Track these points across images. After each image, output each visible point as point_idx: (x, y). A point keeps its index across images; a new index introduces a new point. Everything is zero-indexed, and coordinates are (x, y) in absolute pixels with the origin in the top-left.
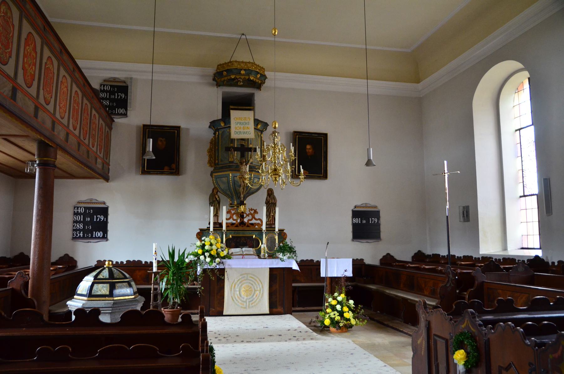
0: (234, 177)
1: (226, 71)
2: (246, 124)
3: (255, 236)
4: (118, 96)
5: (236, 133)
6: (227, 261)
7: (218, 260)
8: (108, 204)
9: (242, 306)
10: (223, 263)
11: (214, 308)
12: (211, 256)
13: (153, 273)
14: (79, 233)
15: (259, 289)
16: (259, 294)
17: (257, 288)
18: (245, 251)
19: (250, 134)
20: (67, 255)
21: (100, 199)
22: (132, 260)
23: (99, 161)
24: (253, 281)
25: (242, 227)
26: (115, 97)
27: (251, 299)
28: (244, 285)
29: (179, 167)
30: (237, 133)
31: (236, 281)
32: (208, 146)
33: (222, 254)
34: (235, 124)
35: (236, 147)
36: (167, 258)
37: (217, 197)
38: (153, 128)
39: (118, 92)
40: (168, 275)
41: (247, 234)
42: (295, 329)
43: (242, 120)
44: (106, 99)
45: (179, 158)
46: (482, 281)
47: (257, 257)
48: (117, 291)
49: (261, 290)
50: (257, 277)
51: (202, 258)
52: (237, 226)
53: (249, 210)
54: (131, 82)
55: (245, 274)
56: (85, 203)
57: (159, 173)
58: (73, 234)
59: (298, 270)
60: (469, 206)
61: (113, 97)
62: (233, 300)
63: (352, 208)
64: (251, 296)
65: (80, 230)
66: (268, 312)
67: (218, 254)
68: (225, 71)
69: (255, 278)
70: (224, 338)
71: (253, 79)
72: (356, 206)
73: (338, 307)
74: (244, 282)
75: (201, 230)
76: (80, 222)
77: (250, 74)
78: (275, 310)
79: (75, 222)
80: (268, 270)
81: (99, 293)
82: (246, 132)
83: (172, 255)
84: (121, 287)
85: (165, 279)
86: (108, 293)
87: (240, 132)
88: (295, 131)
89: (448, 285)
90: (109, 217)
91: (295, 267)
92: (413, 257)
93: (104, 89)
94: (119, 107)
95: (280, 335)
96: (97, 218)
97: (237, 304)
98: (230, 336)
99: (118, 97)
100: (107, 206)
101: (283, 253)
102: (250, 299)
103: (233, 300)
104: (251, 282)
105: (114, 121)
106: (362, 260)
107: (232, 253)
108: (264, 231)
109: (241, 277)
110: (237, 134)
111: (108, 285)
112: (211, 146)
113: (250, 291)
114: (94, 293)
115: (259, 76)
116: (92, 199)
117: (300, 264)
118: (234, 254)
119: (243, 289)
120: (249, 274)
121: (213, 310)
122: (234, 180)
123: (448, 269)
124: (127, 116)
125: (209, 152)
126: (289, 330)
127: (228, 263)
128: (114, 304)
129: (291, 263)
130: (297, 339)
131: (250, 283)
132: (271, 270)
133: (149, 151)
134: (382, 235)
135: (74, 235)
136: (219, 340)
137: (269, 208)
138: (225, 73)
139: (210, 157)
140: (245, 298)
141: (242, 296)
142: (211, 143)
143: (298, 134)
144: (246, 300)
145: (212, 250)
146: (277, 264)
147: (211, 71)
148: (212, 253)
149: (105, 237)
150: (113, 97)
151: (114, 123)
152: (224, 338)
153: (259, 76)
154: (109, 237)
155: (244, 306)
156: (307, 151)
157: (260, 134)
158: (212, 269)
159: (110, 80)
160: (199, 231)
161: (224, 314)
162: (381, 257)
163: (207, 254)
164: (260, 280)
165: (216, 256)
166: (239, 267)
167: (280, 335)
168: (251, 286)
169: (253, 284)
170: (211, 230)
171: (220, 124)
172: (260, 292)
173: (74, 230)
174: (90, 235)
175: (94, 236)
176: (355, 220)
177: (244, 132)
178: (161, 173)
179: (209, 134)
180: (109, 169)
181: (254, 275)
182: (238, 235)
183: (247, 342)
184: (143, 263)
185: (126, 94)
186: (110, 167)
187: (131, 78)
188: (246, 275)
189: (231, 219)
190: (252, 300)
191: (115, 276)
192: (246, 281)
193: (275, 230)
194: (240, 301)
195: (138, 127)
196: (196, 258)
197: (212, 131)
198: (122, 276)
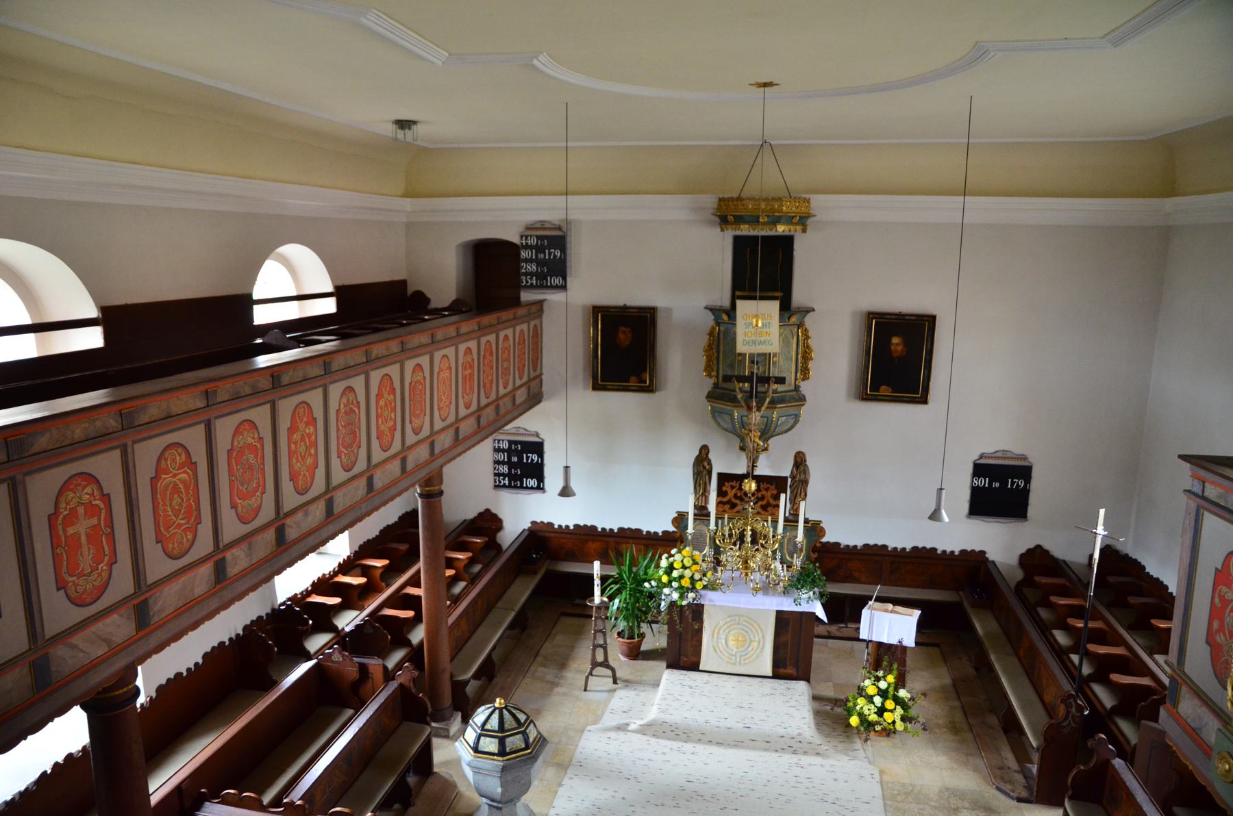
0: (742, 416)
4: (550, 254)
5: (746, 343)
6: (710, 595)
11: (687, 658)
14: (504, 480)
15: (757, 639)
17: (754, 637)
19: (772, 344)
20: (488, 511)
21: (532, 427)
22: (582, 524)
24: (748, 627)
27: (744, 653)
32: (704, 341)
34: (745, 326)
37: (706, 464)
38: (610, 310)
42: (793, 736)
55: (736, 615)
56: (509, 434)
57: (621, 388)
58: (495, 480)
61: (542, 256)
62: (716, 651)
63: (976, 457)
64: (743, 649)
65: (504, 475)
66: (771, 674)
69: (752, 622)
72: (983, 454)
73: (878, 700)
74: (735, 626)
76: (503, 463)
78: (782, 671)
79: (497, 462)
80: (775, 614)
82: (765, 342)
89: (1065, 724)
90: (546, 457)
94: (553, 274)
95: (767, 742)
98: (692, 732)
99: (550, 256)
100: (540, 440)
102: (742, 652)
103: (716, 651)
104: (745, 628)
106: (983, 553)
109: (729, 619)
110: (747, 346)
111: (496, 741)
112: (710, 340)
119: (731, 638)
120: (743, 616)
121: (685, 659)
122: (742, 422)
123: (1070, 699)
125: (706, 351)
126: (782, 737)
131: (743, 630)
134: (1031, 511)
135: (496, 482)
136: (677, 735)
140: (735, 650)
141: (730, 646)
144: (736, 653)
147: (710, 201)
150: (542, 256)
154: (546, 487)
155: (731, 662)
156: (893, 348)
160: (676, 515)
161: (700, 668)
162: (1023, 551)
163: (675, 584)
167: (767, 742)
168: (745, 634)
173: (495, 475)
174: (519, 482)
176: (978, 482)
177: (761, 341)
184: (600, 530)
185: (563, 250)
188: (736, 616)
190: (746, 654)
192: (738, 626)
194: (726, 654)
195: (584, 307)
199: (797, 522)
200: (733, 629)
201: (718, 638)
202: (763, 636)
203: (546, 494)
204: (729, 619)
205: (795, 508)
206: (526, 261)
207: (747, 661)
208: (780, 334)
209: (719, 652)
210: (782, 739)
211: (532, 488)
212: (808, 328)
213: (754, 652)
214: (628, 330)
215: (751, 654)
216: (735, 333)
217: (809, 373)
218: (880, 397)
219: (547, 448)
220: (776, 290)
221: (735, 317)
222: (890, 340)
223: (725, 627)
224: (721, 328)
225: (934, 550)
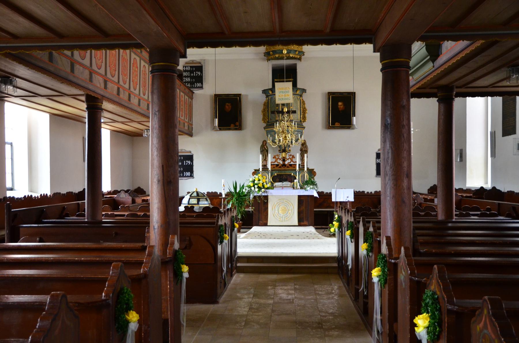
1: (272, 51)
2: (287, 92)
3: (293, 174)
4: (196, 74)
7: (263, 190)
8: (193, 153)
9: (279, 220)
10: (266, 192)
12: (258, 187)
13: (222, 198)
14: (188, 84)
16: (291, 213)
17: (290, 208)
18: (285, 184)
21: (188, 149)
23: (186, 124)
24: (287, 204)
25: (284, 167)
26: (194, 75)
27: (286, 216)
28: (281, 206)
29: (241, 124)
30: (280, 99)
31: (275, 204)
32: (262, 107)
33: (266, 186)
35: (281, 111)
36: (233, 190)
37: (266, 147)
38: (222, 96)
39: (195, 71)
40: (233, 200)
41: (288, 173)
43: (284, 89)
44: (188, 77)
45: (241, 118)
46: (420, 202)
47: (292, 188)
48: (200, 203)
49: (293, 210)
50: (290, 201)
51: (253, 188)
52: (280, 167)
53: (289, 156)
54: (204, 63)
55: (282, 199)
57: (227, 129)
59: (317, 197)
60: (462, 149)
61: (192, 75)
62: (274, 216)
67: (263, 186)
68: (271, 51)
69: (288, 202)
70: (264, 236)
71: (293, 56)
75: (255, 170)
77: (290, 53)
78: (302, 223)
80: (297, 197)
81: (193, 203)
82: (287, 99)
83: (235, 188)
84: (203, 201)
85: (231, 203)
86: (196, 203)
87: (283, 99)
88: (329, 91)
91: (316, 195)
92: (429, 190)
93: (186, 70)
94: (197, 82)
96: (186, 163)
97: (276, 219)
98: (267, 235)
99: (196, 74)
100: (192, 154)
101: (307, 185)
102: (285, 215)
103: (274, 216)
104: (286, 205)
105: (194, 93)
107: (276, 186)
108: (298, 170)
109: (279, 201)
111: (196, 199)
112: (264, 107)
113: (285, 210)
114: (190, 203)
115: (297, 53)
116: (182, 149)
117: (318, 193)
118: (276, 186)
119: (280, 209)
120: (284, 199)
121: (261, 222)
124: (203, 89)
126: (304, 232)
127: (271, 193)
128: (199, 208)
129: (312, 192)
130: (309, 238)
132: (299, 197)
133: (216, 126)
137: (302, 154)
138: (271, 53)
139: (264, 115)
140: (282, 215)
142: (264, 105)
143: (332, 94)
144: (282, 216)
145: (259, 183)
146: (303, 193)
148: (259, 185)
149: (192, 176)
150: (192, 75)
151: (194, 95)
152: (264, 236)
153: (297, 53)
154: (194, 176)
156: (339, 107)
157: (299, 97)
158: (259, 196)
159: (189, 62)
160: (254, 171)
161: (268, 225)
163: (256, 186)
164: (292, 204)
165: (262, 187)
166: (277, 194)
169: (287, 206)
170: (305, 170)
171: (269, 92)
172: (292, 211)
174: (182, 174)
175: (185, 175)
176: (379, 161)
178: (228, 129)
179: (263, 98)
180: (192, 127)
181: (287, 200)
182: (281, 173)
183: (278, 239)
184: (219, 194)
185: (202, 72)
186: (193, 126)
187: (204, 60)
188: (283, 200)
189: (276, 162)
190: (286, 216)
191: (200, 195)
192: (282, 204)
193: (304, 170)
194: (278, 217)
195: (211, 96)
196: (249, 189)
197: (264, 96)
198: (203, 195)
199: (304, 168)
200: (281, 205)
201: (275, 210)
202: (293, 208)
203: (194, 179)
204: (279, 201)
205: (303, 162)
206: (185, 77)
207: (287, 219)
208: (293, 98)
209: (275, 216)
210: (304, 233)
211: (188, 176)
212: (304, 101)
213: (290, 215)
214: (229, 104)
215: (289, 215)
216: (275, 98)
217: (306, 119)
218: (335, 127)
219: (195, 158)
220: (291, 78)
221: (275, 91)
222: (338, 104)
223: (277, 205)
224: (269, 98)
225: (364, 192)
